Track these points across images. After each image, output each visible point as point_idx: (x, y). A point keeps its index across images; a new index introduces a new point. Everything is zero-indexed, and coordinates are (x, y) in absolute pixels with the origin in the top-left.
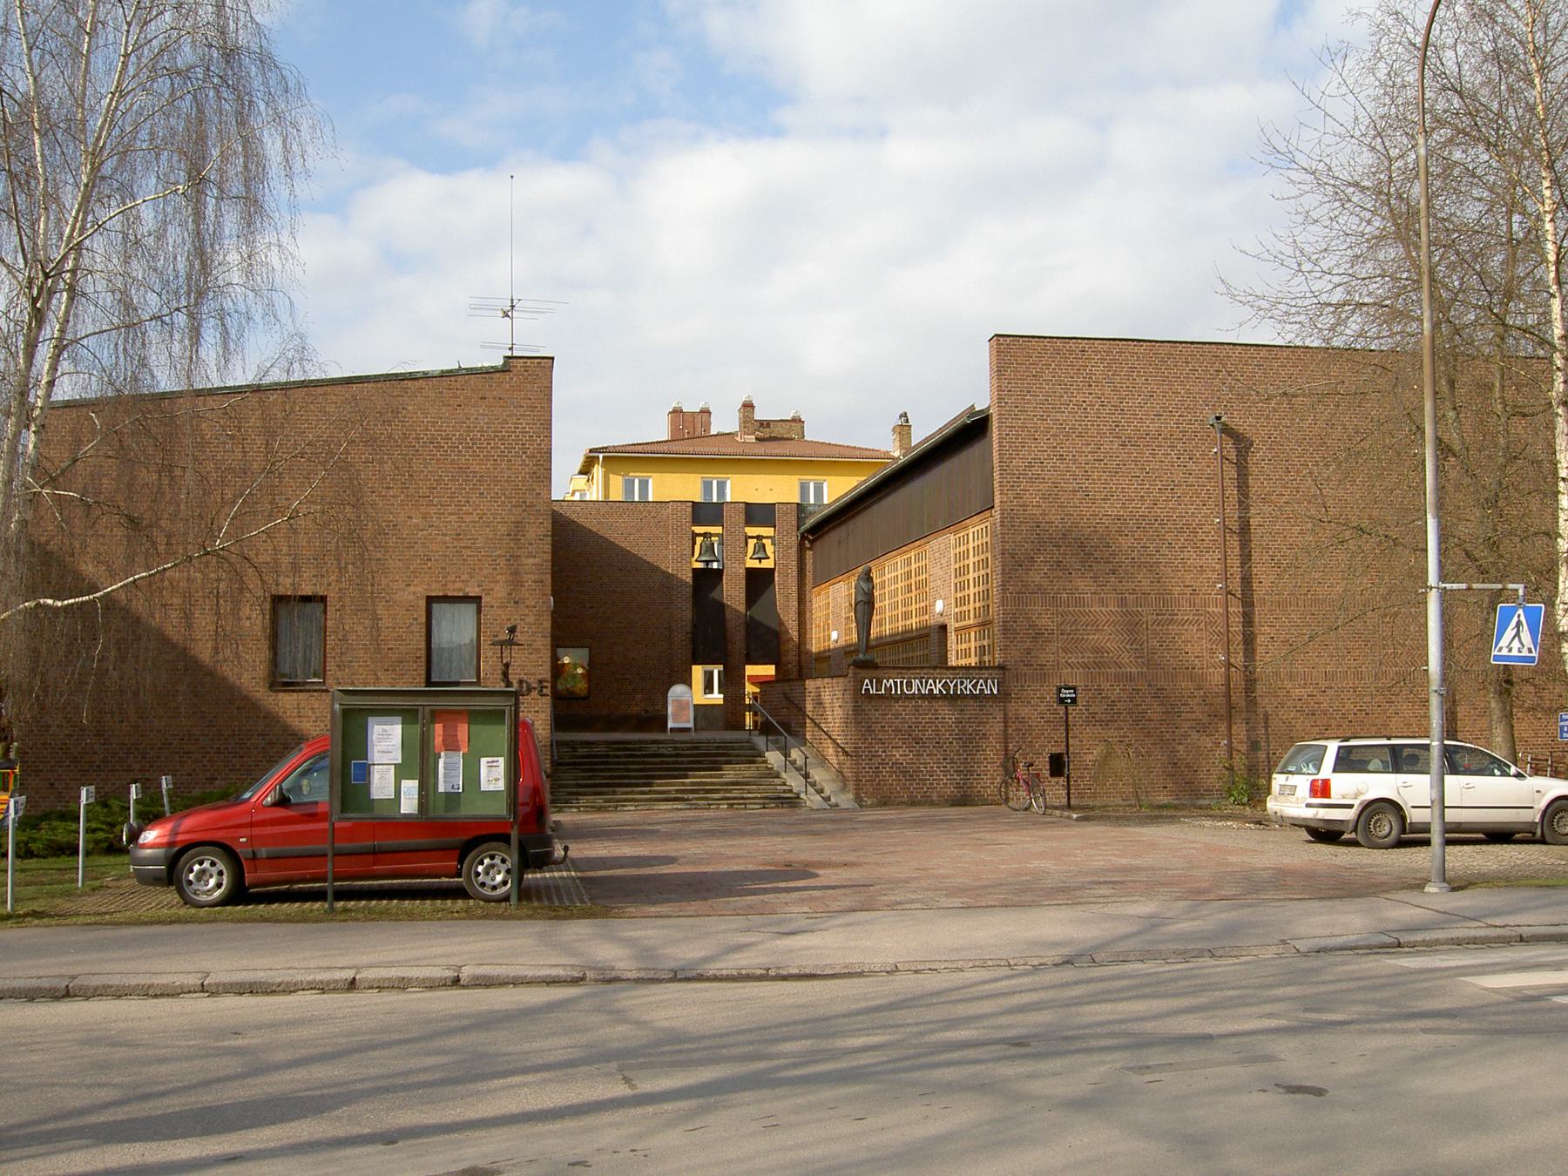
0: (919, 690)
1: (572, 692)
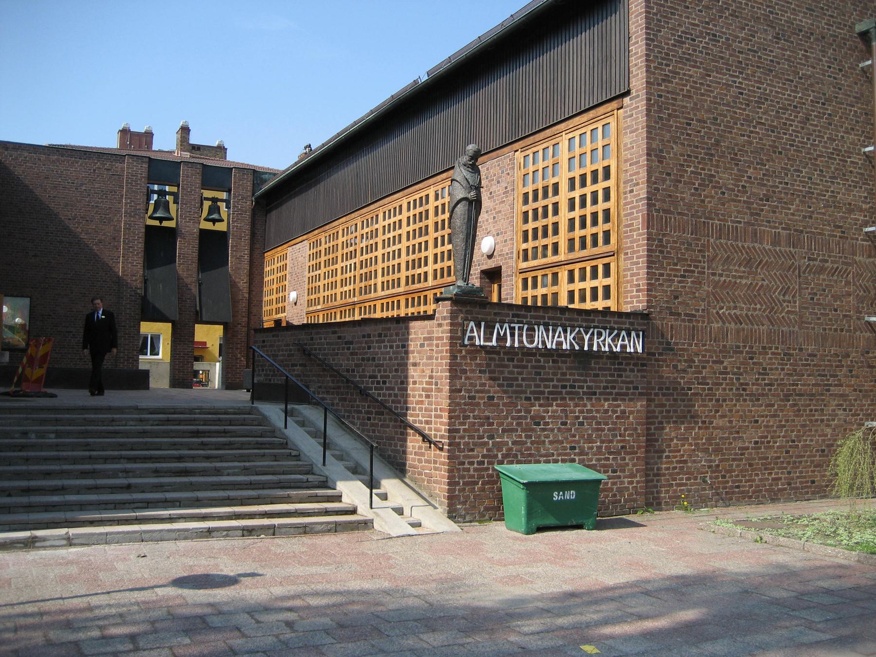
0: (544, 343)
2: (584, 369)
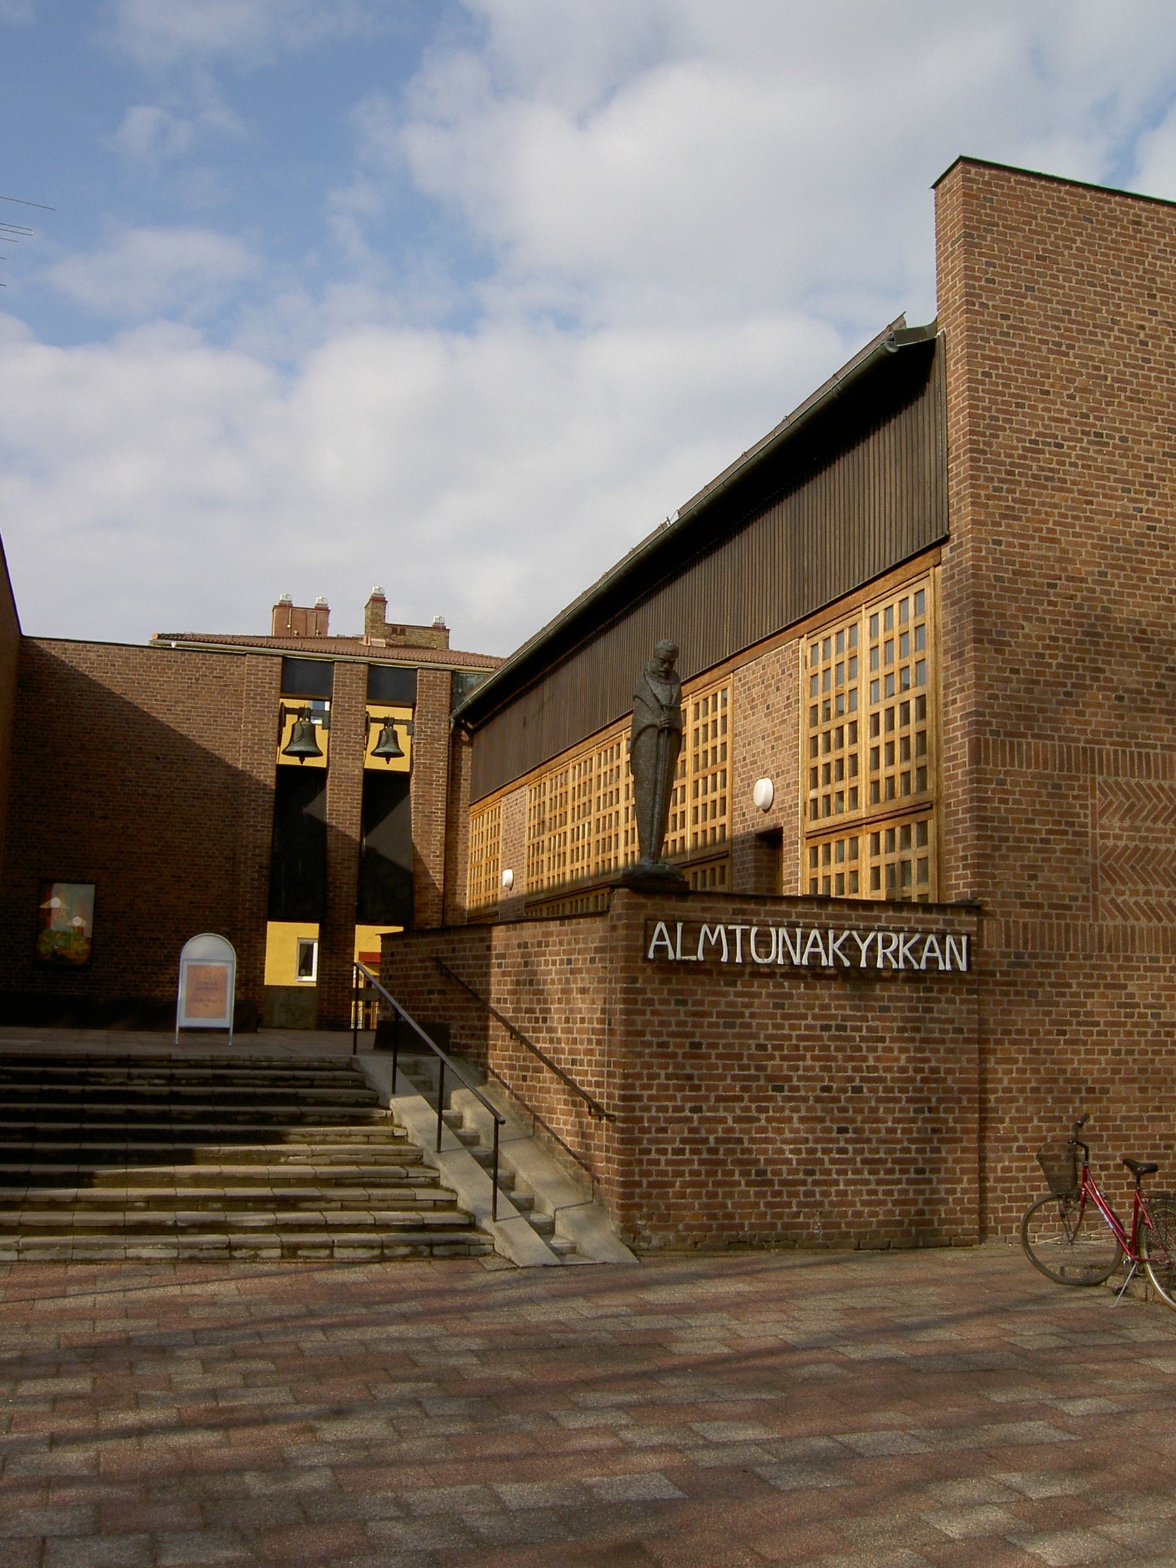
0: (787, 955)
1: (63, 957)
2: (861, 998)
